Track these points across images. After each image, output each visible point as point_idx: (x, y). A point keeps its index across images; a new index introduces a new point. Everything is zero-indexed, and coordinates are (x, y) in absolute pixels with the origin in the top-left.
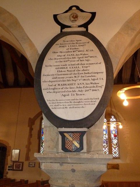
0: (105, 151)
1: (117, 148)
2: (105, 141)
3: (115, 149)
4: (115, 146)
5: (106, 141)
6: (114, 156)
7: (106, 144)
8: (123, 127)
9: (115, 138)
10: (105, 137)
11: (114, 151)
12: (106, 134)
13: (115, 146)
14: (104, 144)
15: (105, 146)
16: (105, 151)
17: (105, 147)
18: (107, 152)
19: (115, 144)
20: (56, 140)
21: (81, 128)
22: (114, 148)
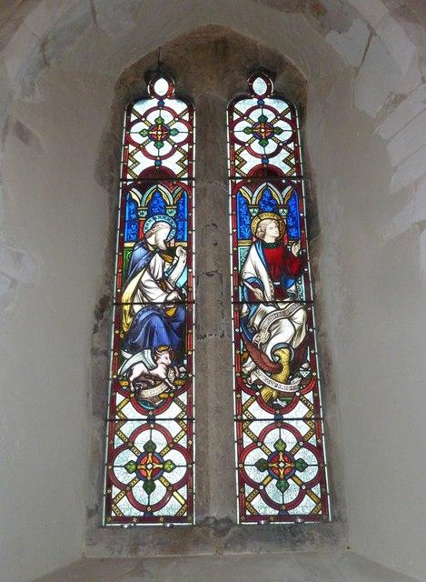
0: (150, 446)
1: (301, 410)
2: (157, 322)
3: (279, 423)
4: (277, 385)
5: (168, 322)
6: (125, 507)
7: (165, 358)
8: (157, 78)
9: (280, 293)
10: (162, 283)
11: (141, 441)
12: (171, 252)
13: (277, 385)
14: (137, 364)
15: (149, 379)
16: (150, 446)
17: (148, 394)
18: (176, 457)
19: (284, 356)
20: (210, 383)
21: (270, 276)
22: (267, 405)
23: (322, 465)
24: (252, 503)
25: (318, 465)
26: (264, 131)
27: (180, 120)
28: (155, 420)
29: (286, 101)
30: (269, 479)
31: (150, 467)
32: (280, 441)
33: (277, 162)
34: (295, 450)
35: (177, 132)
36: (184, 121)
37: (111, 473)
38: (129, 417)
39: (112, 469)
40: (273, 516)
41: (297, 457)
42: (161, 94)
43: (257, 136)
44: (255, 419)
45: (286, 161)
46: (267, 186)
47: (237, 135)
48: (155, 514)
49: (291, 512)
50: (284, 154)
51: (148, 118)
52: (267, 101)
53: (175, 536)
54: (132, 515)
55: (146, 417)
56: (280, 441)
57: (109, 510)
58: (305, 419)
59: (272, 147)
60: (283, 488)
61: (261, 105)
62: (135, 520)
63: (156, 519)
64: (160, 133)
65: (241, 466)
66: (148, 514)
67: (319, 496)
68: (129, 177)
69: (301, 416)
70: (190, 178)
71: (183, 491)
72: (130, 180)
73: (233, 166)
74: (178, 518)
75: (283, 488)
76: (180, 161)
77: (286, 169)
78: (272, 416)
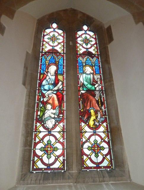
1: (102, 129)
3: (95, 134)
23: (64, 149)
24: (86, 162)
25: (63, 149)
26: (86, 41)
27: (61, 35)
28: (51, 132)
29: (93, 32)
30: (92, 153)
31: (48, 149)
32: (49, 140)
33: (91, 50)
34: (90, 143)
35: (92, 41)
36: (62, 36)
37: (34, 152)
38: (102, 133)
39: (83, 149)
40: (44, 168)
41: (101, 145)
42: (85, 30)
43: (85, 42)
44: (103, 132)
45: (94, 50)
46: (88, 57)
47: (62, 38)
48: (100, 165)
49: (51, 167)
50: (93, 48)
51: (82, 36)
52: (88, 32)
53: (50, 175)
54: (92, 166)
55: (97, 133)
56: (49, 140)
57: (33, 166)
58: (103, 132)
59: (89, 46)
60: (97, 156)
61: (86, 33)
62: (43, 169)
63: (100, 167)
64: (53, 39)
65: (34, 149)
66: (98, 165)
67: (110, 160)
68: (43, 51)
69: (41, 133)
70: (64, 53)
71: (108, 157)
72: (44, 52)
73: (43, 49)
74: (58, 169)
75: (97, 156)
76: (94, 49)
77: (94, 52)
78: (92, 131)
